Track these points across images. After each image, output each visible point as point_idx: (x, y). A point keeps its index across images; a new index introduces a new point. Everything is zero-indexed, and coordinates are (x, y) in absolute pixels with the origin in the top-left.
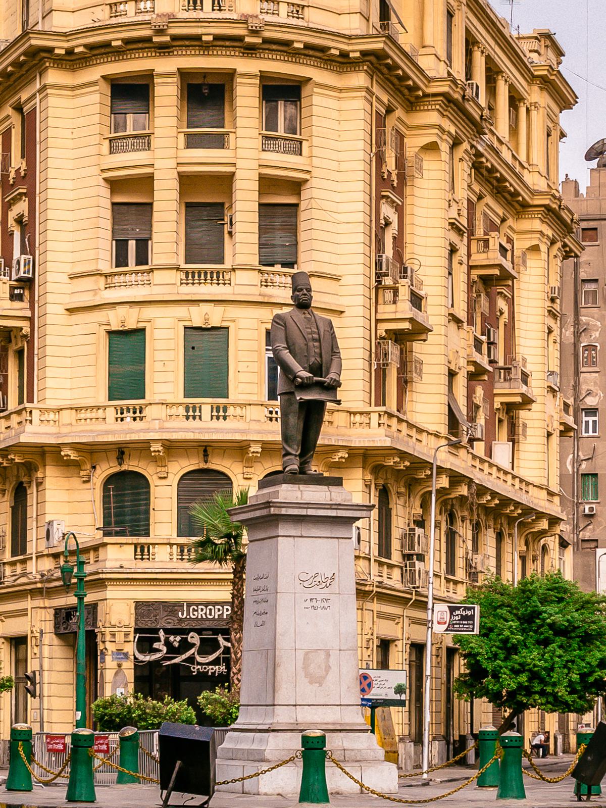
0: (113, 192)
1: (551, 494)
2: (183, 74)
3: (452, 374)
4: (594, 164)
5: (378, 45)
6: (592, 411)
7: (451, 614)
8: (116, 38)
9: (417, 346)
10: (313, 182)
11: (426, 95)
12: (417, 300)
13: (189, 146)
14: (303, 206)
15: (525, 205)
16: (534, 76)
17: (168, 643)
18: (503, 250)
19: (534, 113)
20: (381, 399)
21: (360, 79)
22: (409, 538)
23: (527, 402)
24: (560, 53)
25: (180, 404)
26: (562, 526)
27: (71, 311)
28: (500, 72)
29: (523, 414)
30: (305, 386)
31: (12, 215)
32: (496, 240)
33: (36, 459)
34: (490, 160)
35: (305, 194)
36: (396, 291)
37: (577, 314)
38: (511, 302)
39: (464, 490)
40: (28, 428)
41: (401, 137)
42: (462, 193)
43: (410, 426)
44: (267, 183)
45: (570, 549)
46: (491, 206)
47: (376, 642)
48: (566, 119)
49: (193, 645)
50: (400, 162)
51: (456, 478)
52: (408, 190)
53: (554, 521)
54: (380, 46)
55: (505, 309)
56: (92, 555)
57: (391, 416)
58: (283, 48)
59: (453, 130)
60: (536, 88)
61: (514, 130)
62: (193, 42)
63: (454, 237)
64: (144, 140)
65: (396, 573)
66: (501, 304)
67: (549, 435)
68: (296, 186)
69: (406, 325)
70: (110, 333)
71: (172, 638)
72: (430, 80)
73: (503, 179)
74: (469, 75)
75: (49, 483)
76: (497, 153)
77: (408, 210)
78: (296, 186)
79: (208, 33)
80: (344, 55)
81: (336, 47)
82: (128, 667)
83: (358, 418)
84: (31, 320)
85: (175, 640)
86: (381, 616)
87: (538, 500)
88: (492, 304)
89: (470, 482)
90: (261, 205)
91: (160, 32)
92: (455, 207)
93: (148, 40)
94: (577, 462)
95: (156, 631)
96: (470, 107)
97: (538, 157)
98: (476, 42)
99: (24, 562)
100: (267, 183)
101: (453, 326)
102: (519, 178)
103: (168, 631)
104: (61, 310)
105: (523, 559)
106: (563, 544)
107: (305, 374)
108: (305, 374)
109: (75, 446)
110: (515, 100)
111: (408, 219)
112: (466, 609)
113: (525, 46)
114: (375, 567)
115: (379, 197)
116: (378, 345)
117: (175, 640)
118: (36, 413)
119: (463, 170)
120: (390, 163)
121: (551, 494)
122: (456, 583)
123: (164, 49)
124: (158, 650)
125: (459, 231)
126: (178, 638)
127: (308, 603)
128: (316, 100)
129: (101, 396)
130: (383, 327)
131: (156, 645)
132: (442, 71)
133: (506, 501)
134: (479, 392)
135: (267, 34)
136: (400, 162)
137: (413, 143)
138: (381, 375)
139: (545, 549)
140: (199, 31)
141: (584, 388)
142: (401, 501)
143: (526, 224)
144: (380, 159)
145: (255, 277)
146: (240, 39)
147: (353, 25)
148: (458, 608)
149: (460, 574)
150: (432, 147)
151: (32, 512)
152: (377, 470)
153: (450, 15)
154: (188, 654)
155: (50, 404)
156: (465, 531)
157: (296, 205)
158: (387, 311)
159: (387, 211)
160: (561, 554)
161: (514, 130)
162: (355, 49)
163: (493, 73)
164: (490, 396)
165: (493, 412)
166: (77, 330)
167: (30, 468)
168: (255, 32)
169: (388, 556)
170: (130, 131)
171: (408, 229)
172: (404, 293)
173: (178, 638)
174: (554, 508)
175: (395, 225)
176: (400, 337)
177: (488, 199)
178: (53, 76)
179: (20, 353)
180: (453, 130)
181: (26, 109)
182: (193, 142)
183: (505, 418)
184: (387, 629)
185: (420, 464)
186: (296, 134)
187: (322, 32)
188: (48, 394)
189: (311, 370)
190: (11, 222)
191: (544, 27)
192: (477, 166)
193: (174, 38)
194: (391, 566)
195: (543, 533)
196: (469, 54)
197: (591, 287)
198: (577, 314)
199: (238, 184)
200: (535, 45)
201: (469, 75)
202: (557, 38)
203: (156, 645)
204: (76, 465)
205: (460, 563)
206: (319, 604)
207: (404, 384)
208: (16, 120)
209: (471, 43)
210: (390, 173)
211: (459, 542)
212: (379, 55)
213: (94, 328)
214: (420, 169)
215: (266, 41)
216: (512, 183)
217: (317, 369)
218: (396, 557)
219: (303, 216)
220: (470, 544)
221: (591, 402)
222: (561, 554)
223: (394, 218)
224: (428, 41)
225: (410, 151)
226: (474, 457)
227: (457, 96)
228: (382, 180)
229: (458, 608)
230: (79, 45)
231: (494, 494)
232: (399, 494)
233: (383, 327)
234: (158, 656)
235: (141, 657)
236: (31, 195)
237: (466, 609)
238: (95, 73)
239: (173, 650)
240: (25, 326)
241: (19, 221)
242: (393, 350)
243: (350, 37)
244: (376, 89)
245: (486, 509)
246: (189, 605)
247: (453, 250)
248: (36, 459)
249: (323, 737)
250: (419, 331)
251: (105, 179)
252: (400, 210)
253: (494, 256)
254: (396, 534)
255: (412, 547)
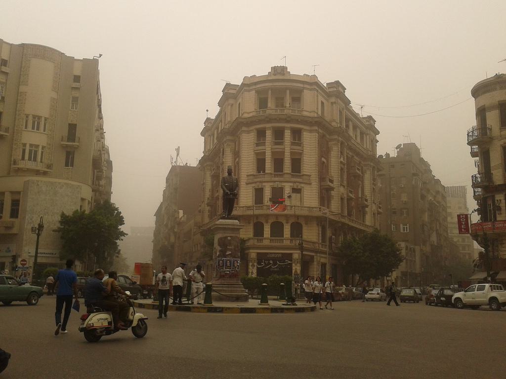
3: (342, 199)
31: (236, 161)
117: (267, 262)
128: (304, 133)
131: (262, 263)
158: (323, 183)
177: (355, 157)
203: (262, 263)
218: (328, 243)
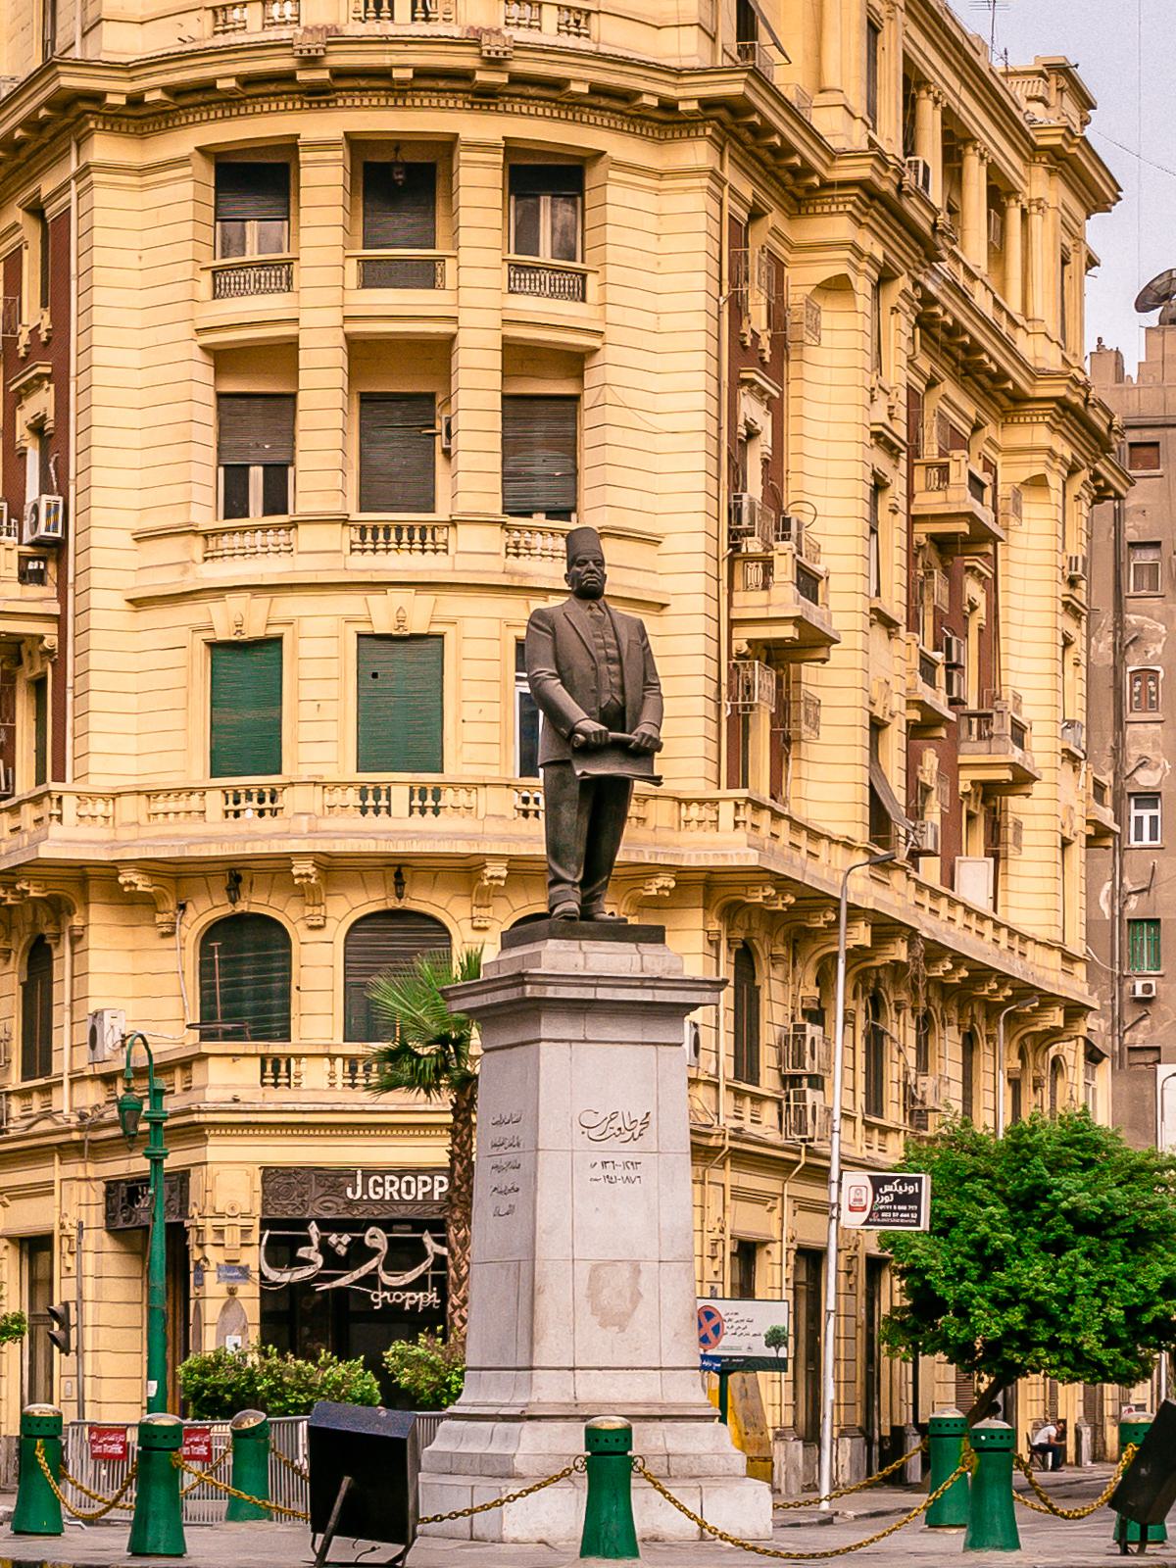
0: (219, 372)
1: (1069, 958)
2: (355, 143)
3: (877, 726)
4: (1153, 318)
5: (733, 87)
6: (1149, 798)
7: (876, 1191)
8: (225, 74)
9: (808, 672)
10: (608, 354)
11: (827, 185)
12: (808, 583)
13: (366, 283)
14: (588, 399)
15: (1019, 399)
16: (1036, 148)
17: (325, 1249)
18: (976, 485)
19: (1036, 220)
20: (739, 775)
21: (698, 153)
22: (794, 1044)
23: (1022, 779)
24: (1086, 103)
25: (350, 784)
26: (1091, 1022)
27: (137, 603)
28: (971, 139)
29: (1014, 803)
30: (591, 749)
31: (24, 417)
32: (962, 465)
33: (69, 891)
34: (950, 311)
35: (591, 377)
36: (768, 565)
37: (1119, 609)
38: (991, 587)
39: (900, 952)
40: (55, 830)
41: (777, 266)
42: (896, 375)
43: (797, 826)
44: (519, 356)
45: (1106, 1065)
46: (954, 400)
47: (730, 1246)
48: (1098, 230)
49: (375, 1252)
50: (777, 315)
51: (886, 929)
52: (791, 369)
53: (1075, 1011)
54: (738, 88)
55: (981, 599)
56: (178, 1076)
57: (758, 806)
58: (549, 92)
59: (878, 252)
60: (1039, 171)
61: (997, 252)
62: (375, 82)
63: (881, 460)
64: (280, 272)
65: (769, 1112)
66: (973, 589)
67: (1066, 843)
68: (575, 362)
69: (788, 632)
70: (213, 646)
71: (333, 1239)
72: (834, 155)
73: (975, 348)
74: (910, 145)
75: (95, 937)
76: (964, 297)
77: (791, 407)
78: (575, 362)
79: (403, 63)
80: (668, 106)
81: (652, 90)
82: (249, 1294)
83: (695, 811)
84: (60, 620)
85: (340, 1242)
86: (740, 1194)
87: (1043, 970)
88: (956, 590)
89: (911, 935)
90: (506, 398)
91: (311, 61)
92: (882, 401)
93: (288, 77)
94: (1120, 896)
95: (303, 1224)
96: (912, 208)
97: (1043, 305)
98: (923, 82)
99: (46, 1090)
100: (519, 356)
101: (879, 633)
102: (1008, 345)
103: (325, 1225)
104: (118, 601)
105: (1015, 1084)
106: (1093, 1056)
107: (592, 726)
108: (592, 726)
109: (146, 866)
110: (999, 194)
111: (791, 426)
112: (903, 1181)
113: (1019, 90)
114: (727, 1101)
115: (736, 383)
116: (734, 670)
117: (340, 1242)
118: (69, 802)
119: (899, 331)
120: (758, 317)
121: (1069, 958)
122: (885, 1131)
123: (318, 96)
124: (307, 1262)
125: (891, 448)
126: (346, 1238)
127: (598, 1170)
128: (613, 193)
129: (196, 768)
130: (744, 634)
131: (302, 1252)
132: (857, 137)
133: (982, 973)
134: (931, 760)
135: (518, 66)
136: (777, 315)
137: (802, 278)
138: (739, 727)
139: (1057, 1065)
140: (386, 60)
141: (1133, 753)
142: (778, 973)
143: (1021, 435)
144: (737, 308)
145: (494, 538)
146: (465, 75)
147: (685, 48)
148: (890, 1181)
149: (893, 1115)
150: (838, 286)
151: (61, 993)
152: (731, 912)
153: (873, 29)
154: (364, 1270)
155: (98, 783)
156: (902, 1030)
157: (575, 399)
158: (750, 603)
159: (751, 409)
160: (1090, 1075)
161: (997, 252)
162: (688, 96)
163: (956, 142)
164: (950, 768)
165: (956, 800)
166: (149, 640)
167: (58, 908)
168: (494, 63)
169: (754, 1078)
170: (252, 255)
171: (791, 444)
172: (784, 569)
173: (346, 1238)
174: (1075, 986)
175: (766, 437)
176: (776, 655)
177: (948, 387)
178: (104, 148)
179: (39, 685)
180: (878, 252)
181: (50, 212)
182: (374, 275)
183: (979, 811)
184: (751, 1221)
185: (815, 900)
186: (574, 260)
187: (626, 61)
188: (94, 764)
189: (603, 717)
190: (21, 430)
191: (1055, 53)
192: (925, 323)
193: (339, 74)
194: (758, 1099)
195: (1053, 1034)
196: (910, 104)
197: (1147, 557)
198: (1119, 609)
199: (462, 357)
200: (1038, 88)
201: (910, 145)
202: (1080, 73)
203: (302, 1252)
204: (147, 903)
205: (892, 1093)
206: (620, 1172)
207: (784, 745)
208: (31, 232)
209: (913, 83)
210: (756, 336)
211: (890, 1051)
212: (736, 108)
213: (182, 636)
214: (816, 328)
215: (516, 79)
216: (994, 355)
217: (615, 717)
218: (769, 1082)
219: (587, 419)
220: (911, 1056)
221: (1146, 779)
222: (1090, 1075)
223: (764, 423)
224: (831, 80)
225: (797, 293)
226: (921, 887)
227: (886, 187)
228: (742, 350)
229: (890, 1181)
230: (152, 87)
231: (959, 959)
232: (774, 959)
233: (744, 634)
234: (306, 1272)
235: (273, 1275)
236: (60, 379)
237: (903, 1181)
238: (185, 141)
239: (335, 1262)
240: (49, 632)
241: (37, 428)
242: (763, 680)
243: (678, 73)
244: (729, 173)
245: (944, 989)
246: (367, 1173)
247: (879, 486)
248: (69, 891)
249: (628, 1431)
250: (813, 642)
251: (204, 348)
252: (776, 407)
253: (959, 497)
254: (769, 1036)
255: (799, 1062)
